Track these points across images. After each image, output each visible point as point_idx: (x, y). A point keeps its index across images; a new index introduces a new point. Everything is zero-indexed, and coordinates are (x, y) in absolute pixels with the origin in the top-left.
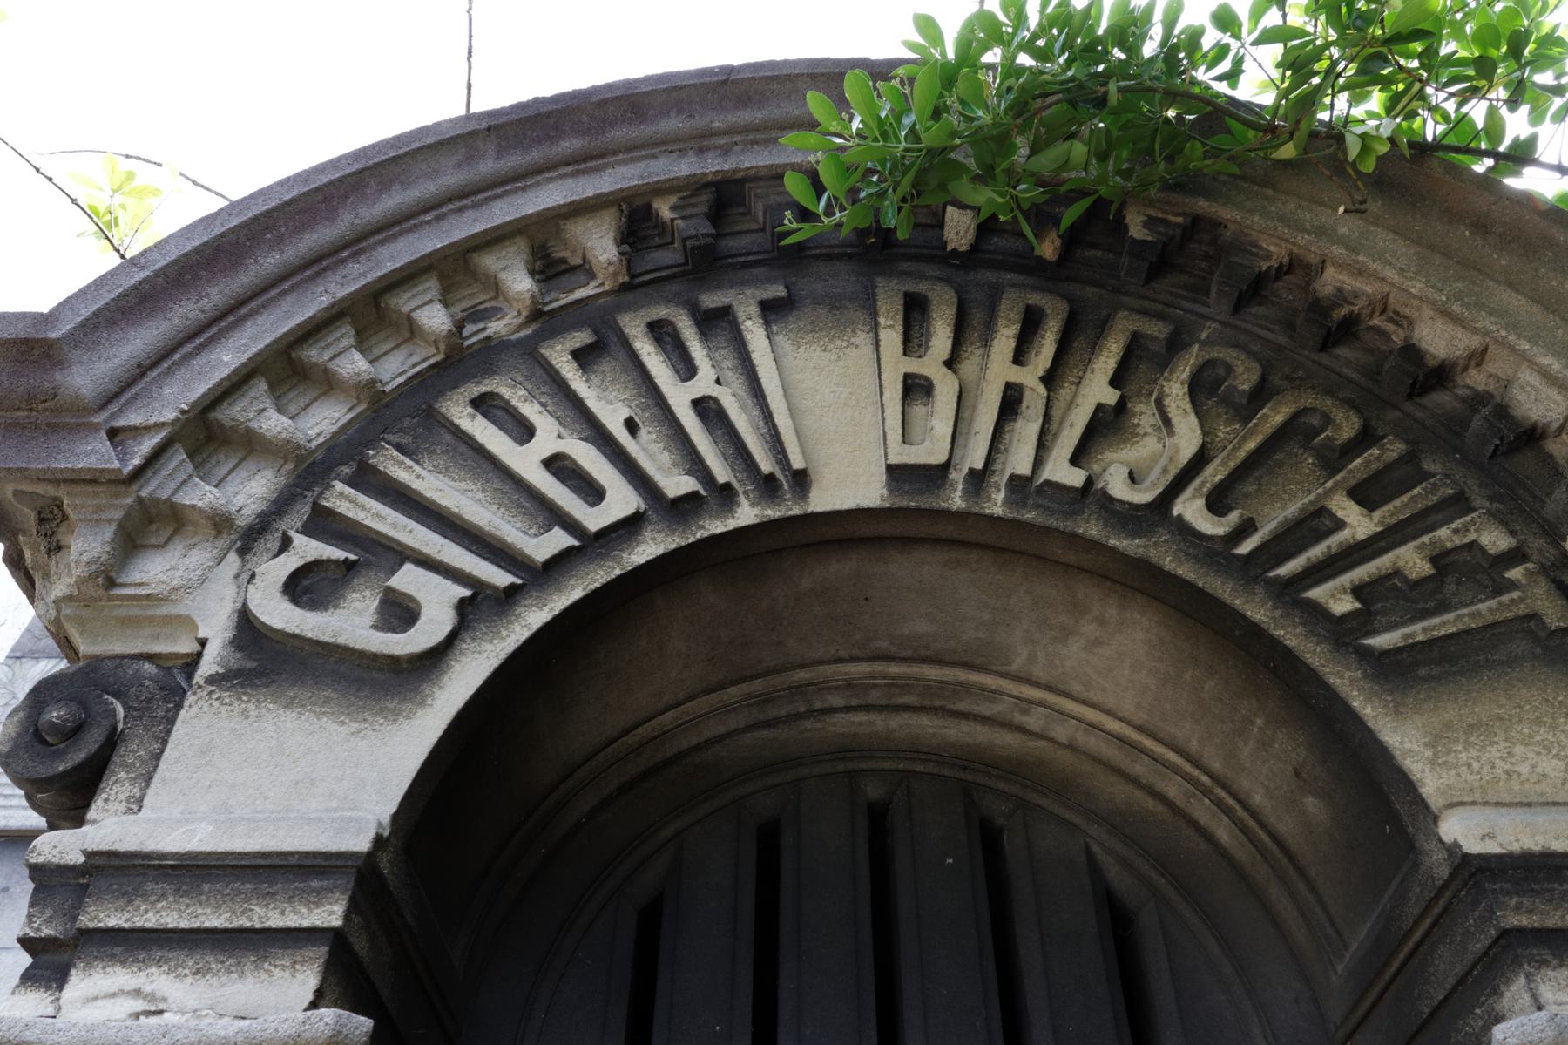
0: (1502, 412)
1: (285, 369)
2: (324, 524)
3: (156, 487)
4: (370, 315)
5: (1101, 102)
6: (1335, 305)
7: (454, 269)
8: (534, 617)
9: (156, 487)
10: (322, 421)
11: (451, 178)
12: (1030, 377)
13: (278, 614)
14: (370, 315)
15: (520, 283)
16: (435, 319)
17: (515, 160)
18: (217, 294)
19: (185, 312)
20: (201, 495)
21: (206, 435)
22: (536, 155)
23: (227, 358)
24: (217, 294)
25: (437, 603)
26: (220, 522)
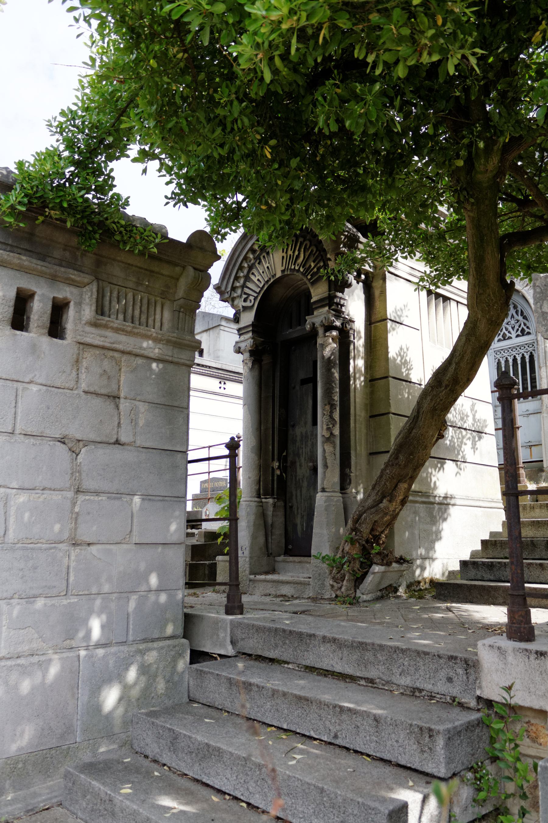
0: (165, 236)
1: (237, 278)
2: (245, 294)
3: (232, 296)
4: (241, 268)
5: (165, 53)
6: (69, 729)
7: (245, 258)
8: (259, 298)
9: (232, 296)
10: (242, 281)
11: (241, 247)
12: (268, 265)
13: (245, 304)
14: (241, 268)
15: (251, 256)
16: (246, 265)
17: (245, 241)
18: (228, 274)
19: (227, 277)
20: (235, 295)
21: (234, 289)
22: (247, 240)
23: (232, 280)
24: (228, 274)
25: (252, 298)
26: (238, 296)
